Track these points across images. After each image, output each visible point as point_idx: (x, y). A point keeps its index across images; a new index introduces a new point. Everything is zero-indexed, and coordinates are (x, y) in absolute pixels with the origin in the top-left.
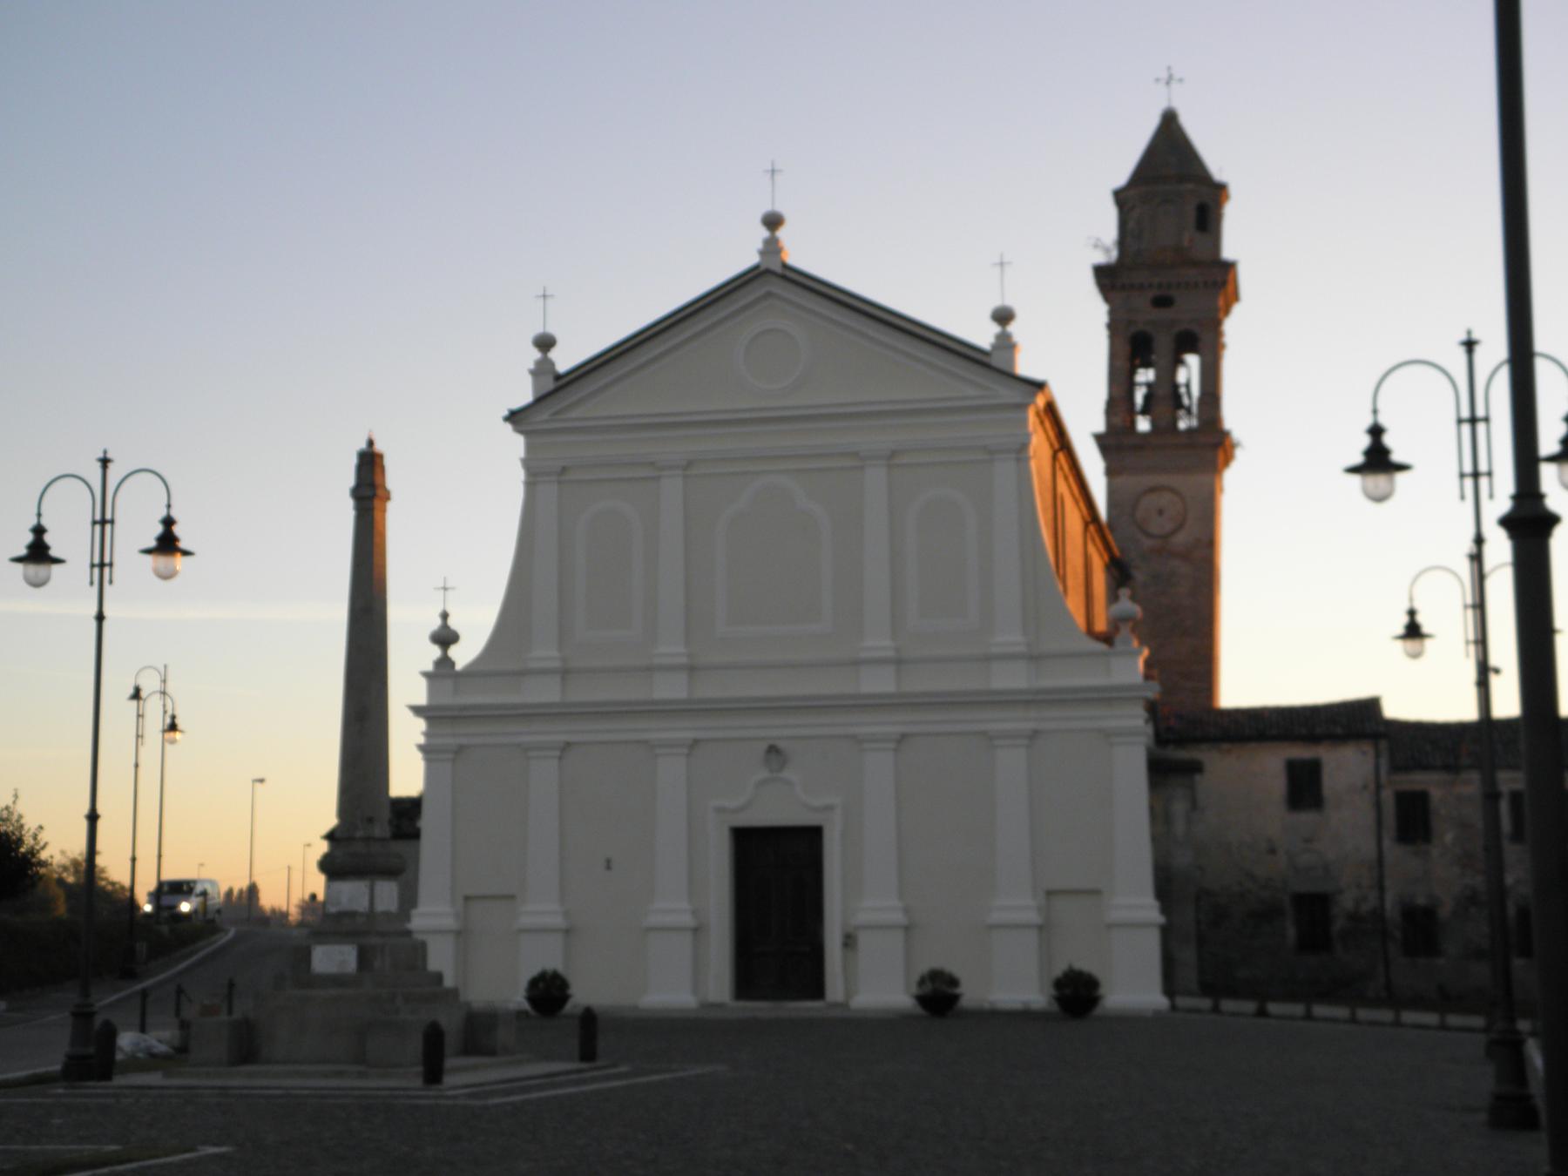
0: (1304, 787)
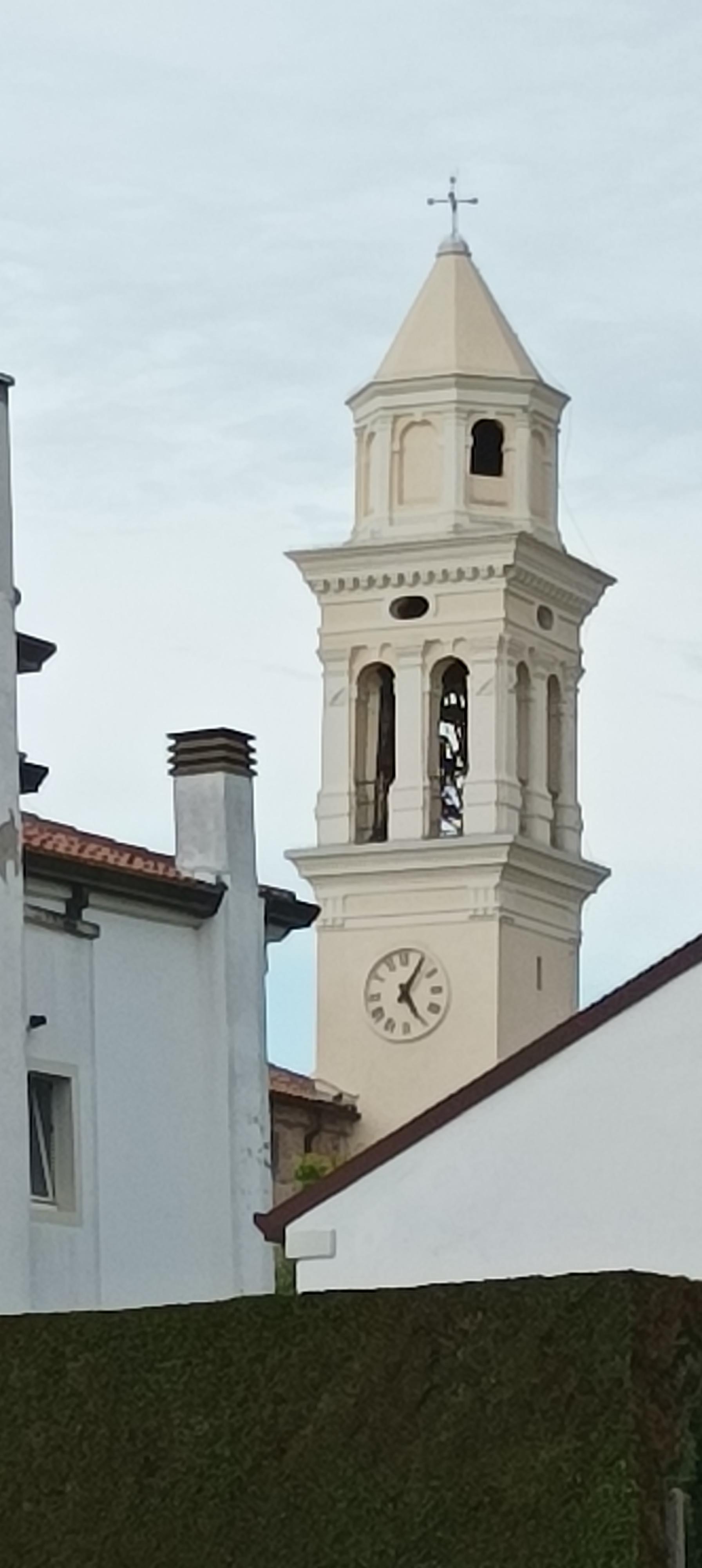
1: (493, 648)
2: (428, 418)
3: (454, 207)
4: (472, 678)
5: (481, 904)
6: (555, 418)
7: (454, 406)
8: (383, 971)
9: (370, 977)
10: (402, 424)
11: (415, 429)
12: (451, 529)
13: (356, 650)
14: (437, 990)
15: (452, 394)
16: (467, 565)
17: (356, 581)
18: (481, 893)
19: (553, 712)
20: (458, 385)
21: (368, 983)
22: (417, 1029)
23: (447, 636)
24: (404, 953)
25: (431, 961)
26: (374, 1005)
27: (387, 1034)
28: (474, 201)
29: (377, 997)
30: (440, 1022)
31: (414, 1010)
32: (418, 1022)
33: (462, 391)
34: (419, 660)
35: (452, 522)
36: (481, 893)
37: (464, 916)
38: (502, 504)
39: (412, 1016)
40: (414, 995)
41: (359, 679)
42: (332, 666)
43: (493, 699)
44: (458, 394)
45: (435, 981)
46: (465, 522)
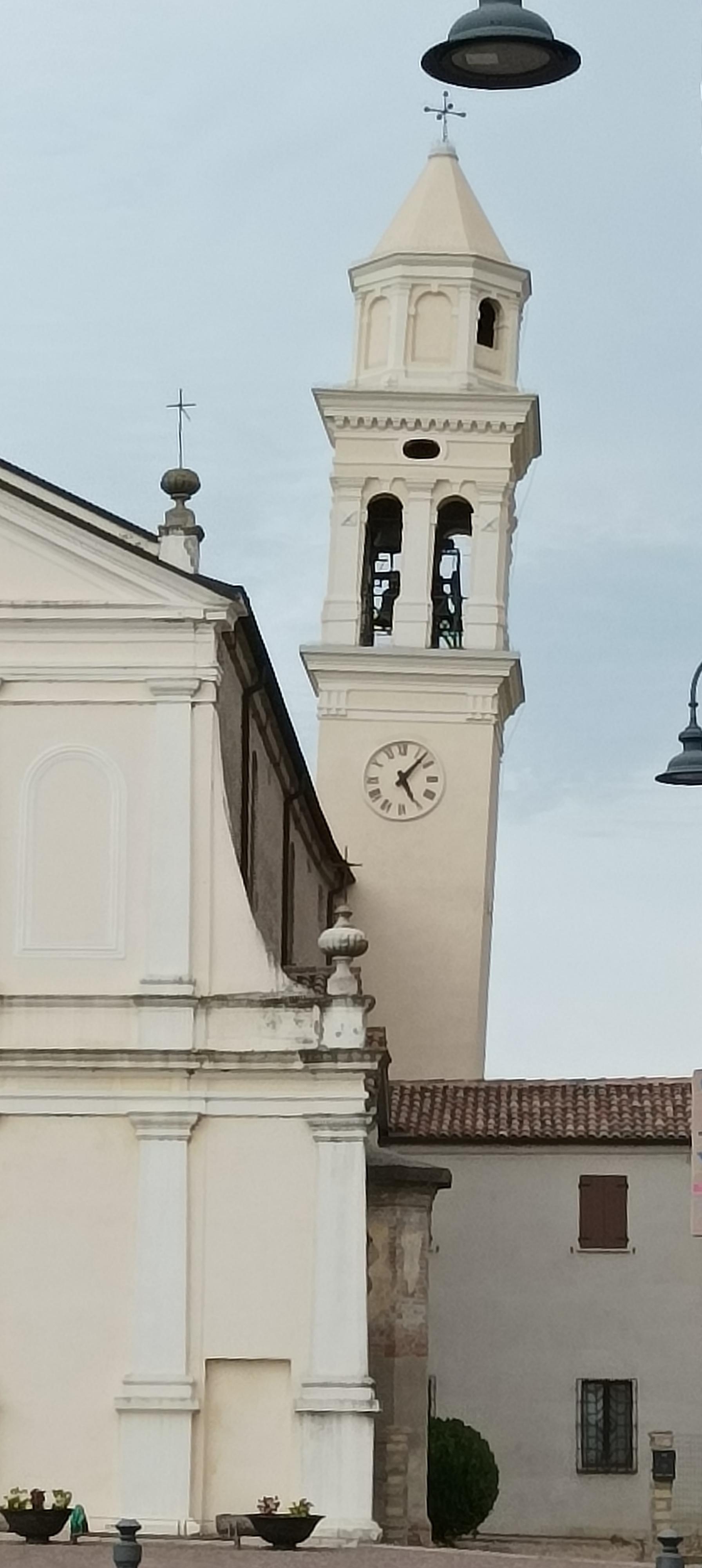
0: (603, 1218)
1: (499, 492)
2: (442, 290)
4: (406, 513)
5: (479, 709)
7: (469, 282)
8: (383, 758)
9: (370, 763)
10: (419, 292)
11: (429, 298)
12: (465, 387)
13: (369, 480)
14: (432, 779)
15: (468, 272)
16: (482, 418)
17: (375, 421)
20: (475, 265)
21: (368, 767)
22: (412, 811)
23: (456, 477)
24: (403, 746)
25: (431, 754)
26: (373, 787)
27: (383, 813)
28: (463, 115)
29: (375, 780)
30: (435, 807)
31: (410, 795)
32: (414, 804)
33: (479, 272)
34: (358, 493)
35: (466, 381)
36: (480, 700)
37: (462, 718)
38: (496, 372)
39: (409, 799)
40: (411, 782)
42: (345, 492)
43: (497, 535)
44: (475, 273)
45: (431, 771)
46: (475, 382)
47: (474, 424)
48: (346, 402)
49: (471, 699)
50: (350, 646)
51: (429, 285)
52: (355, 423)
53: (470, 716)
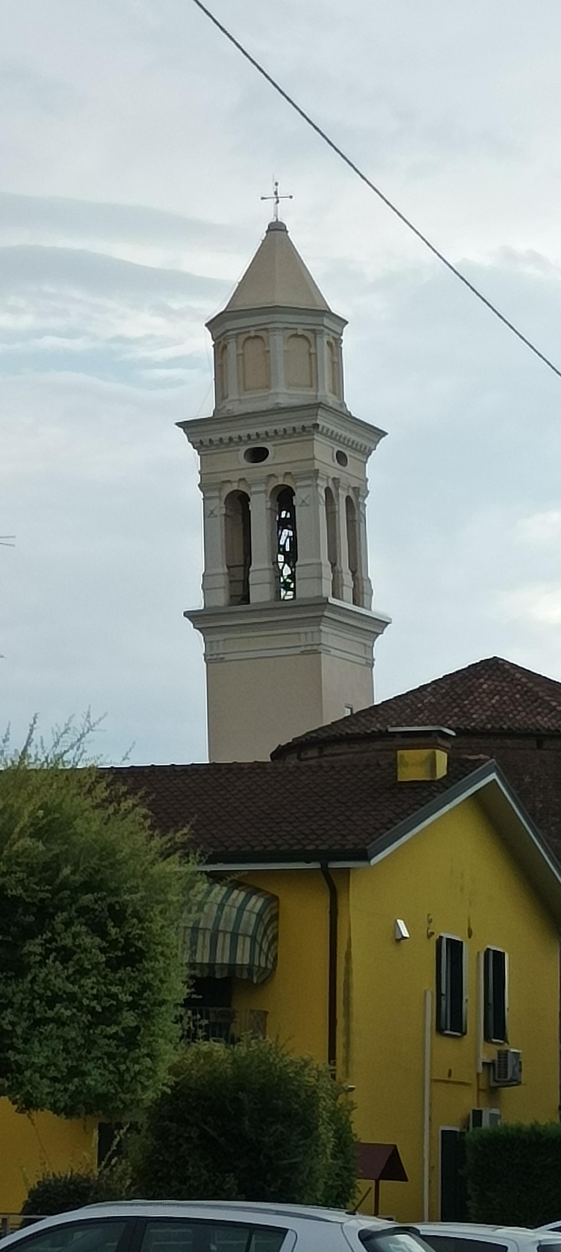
2: (260, 334)
3: (276, 193)
6: (340, 332)
18: (310, 635)
19: (350, 519)
41: (226, 499)
47: (231, 439)
48: (230, 424)
49: (303, 635)
50: (221, 607)
51: (296, 329)
52: (236, 440)
53: (303, 649)
